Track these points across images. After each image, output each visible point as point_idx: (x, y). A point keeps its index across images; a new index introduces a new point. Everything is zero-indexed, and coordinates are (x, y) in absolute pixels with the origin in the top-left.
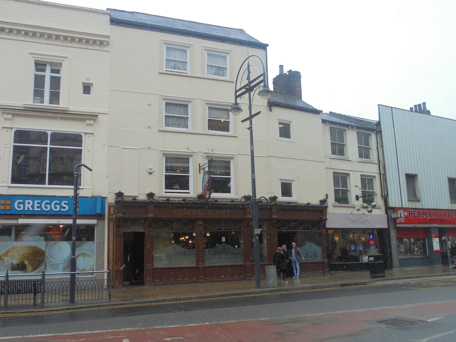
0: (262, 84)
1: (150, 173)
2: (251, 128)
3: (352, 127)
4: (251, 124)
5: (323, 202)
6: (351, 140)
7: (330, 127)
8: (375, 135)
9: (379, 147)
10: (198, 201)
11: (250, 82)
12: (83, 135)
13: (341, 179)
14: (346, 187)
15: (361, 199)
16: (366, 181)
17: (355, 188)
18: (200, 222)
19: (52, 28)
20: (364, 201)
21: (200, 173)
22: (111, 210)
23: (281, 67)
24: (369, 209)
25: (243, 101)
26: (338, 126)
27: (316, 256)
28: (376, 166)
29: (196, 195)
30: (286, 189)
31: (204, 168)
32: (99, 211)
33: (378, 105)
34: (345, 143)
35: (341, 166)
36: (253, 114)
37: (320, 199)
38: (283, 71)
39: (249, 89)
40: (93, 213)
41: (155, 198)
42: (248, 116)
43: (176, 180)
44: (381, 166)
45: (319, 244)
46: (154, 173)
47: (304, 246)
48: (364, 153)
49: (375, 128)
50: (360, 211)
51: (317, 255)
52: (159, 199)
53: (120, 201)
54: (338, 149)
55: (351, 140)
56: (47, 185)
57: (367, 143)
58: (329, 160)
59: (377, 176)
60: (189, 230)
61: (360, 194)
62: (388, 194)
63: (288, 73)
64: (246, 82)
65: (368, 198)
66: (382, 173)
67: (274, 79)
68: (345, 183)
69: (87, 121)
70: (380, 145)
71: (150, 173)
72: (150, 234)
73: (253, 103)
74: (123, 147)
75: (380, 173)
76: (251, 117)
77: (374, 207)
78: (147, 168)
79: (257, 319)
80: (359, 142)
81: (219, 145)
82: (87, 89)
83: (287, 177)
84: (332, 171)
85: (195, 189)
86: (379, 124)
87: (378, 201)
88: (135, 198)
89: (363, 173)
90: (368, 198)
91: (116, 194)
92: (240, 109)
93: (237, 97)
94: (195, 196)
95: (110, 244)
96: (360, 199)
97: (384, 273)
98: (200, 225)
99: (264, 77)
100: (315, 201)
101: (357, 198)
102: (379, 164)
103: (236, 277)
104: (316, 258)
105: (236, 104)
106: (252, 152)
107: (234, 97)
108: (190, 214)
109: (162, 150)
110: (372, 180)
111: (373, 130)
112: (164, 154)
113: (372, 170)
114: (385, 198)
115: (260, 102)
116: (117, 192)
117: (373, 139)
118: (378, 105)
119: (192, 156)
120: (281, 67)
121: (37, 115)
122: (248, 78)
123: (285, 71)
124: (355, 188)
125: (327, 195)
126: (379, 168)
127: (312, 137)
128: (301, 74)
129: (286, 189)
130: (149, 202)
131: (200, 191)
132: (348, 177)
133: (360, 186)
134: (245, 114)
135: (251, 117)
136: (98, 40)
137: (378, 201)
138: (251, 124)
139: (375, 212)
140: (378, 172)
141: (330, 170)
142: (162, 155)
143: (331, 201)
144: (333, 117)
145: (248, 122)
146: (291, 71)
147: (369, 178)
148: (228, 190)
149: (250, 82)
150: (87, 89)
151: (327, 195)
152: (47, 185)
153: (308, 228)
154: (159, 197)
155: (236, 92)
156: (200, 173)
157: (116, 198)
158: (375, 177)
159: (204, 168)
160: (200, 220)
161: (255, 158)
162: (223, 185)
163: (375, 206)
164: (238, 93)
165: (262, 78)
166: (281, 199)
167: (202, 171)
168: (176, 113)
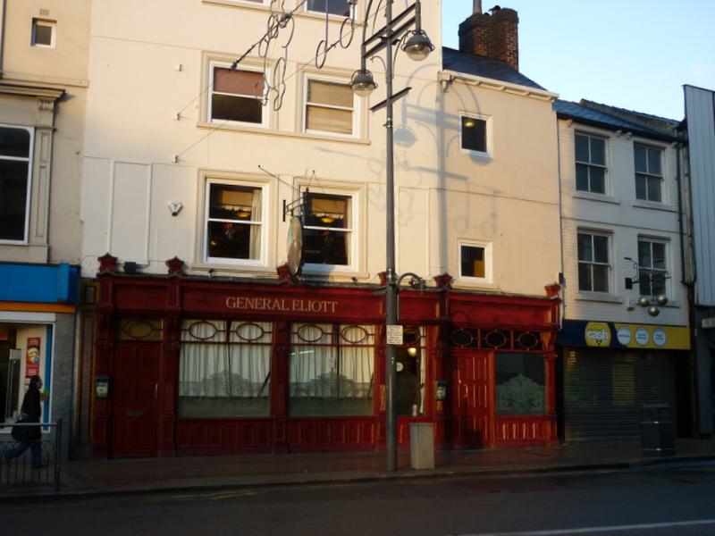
0: (413, 27)
2: (391, 123)
3: (625, 131)
4: (390, 115)
5: (553, 289)
6: (619, 155)
7: (576, 131)
8: (675, 150)
9: (682, 177)
11: (391, 23)
13: (592, 245)
14: (606, 261)
15: (636, 287)
16: (650, 249)
17: (622, 260)
20: (644, 291)
21: (284, 220)
24: (653, 310)
25: (376, 67)
26: (592, 125)
27: (533, 405)
28: (674, 218)
29: (274, 266)
31: (292, 211)
33: (685, 86)
35: (598, 215)
36: (394, 93)
38: (480, 7)
39: (388, 38)
42: (384, 97)
44: (684, 217)
48: (647, 185)
49: (676, 135)
50: (633, 312)
51: (534, 402)
53: (107, 274)
54: (590, 176)
55: (619, 155)
57: (656, 165)
59: (675, 238)
61: (634, 274)
62: (695, 277)
63: (490, 13)
64: (382, 22)
65: (650, 283)
66: (685, 231)
67: (462, 26)
68: (602, 253)
70: (683, 175)
73: (397, 70)
75: (681, 233)
76: (393, 97)
77: (664, 303)
78: (169, 203)
79: (651, 449)
80: (639, 163)
82: (41, 34)
84: (637, 232)
86: (683, 126)
87: (673, 290)
89: (643, 232)
90: (650, 283)
92: (373, 83)
93: (365, 56)
95: (85, 365)
96: (634, 285)
99: (419, 12)
100: (537, 289)
101: (629, 284)
102: (680, 213)
104: (532, 408)
105: (363, 71)
106: (560, 208)
107: (360, 56)
110: (605, 239)
111: (668, 139)
113: (662, 223)
114: (689, 286)
115: (421, 75)
116: (102, 254)
117: (668, 158)
118: (685, 86)
122: (388, 13)
123: (486, 8)
124: (622, 260)
126: (680, 221)
127: (533, 153)
128: (519, 16)
129: (472, 259)
131: (283, 259)
132: (609, 239)
133: (636, 258)
134: (380, 94)
135: (393, 97)
137: (673, 290)
138: (390, 115)
139: (667, 316)
140: (678, 229)
143: (571, 291)
144: (586, 111)
145: (384, 111)
146: (497, 8)
147: (656, 241)
148: (342, 259)
149: (391, 23)
150: (41, 34)
154: (194, 269)
155: (365, 44)
156: (284, 220)
157: (101, 269)
158: (668, 239)
159: (292, 211)
162: (335, 249)
163: (665, 301)
164: (369, 47)
165: (412, 14)
166: (462, 282)
167: (288, 217)
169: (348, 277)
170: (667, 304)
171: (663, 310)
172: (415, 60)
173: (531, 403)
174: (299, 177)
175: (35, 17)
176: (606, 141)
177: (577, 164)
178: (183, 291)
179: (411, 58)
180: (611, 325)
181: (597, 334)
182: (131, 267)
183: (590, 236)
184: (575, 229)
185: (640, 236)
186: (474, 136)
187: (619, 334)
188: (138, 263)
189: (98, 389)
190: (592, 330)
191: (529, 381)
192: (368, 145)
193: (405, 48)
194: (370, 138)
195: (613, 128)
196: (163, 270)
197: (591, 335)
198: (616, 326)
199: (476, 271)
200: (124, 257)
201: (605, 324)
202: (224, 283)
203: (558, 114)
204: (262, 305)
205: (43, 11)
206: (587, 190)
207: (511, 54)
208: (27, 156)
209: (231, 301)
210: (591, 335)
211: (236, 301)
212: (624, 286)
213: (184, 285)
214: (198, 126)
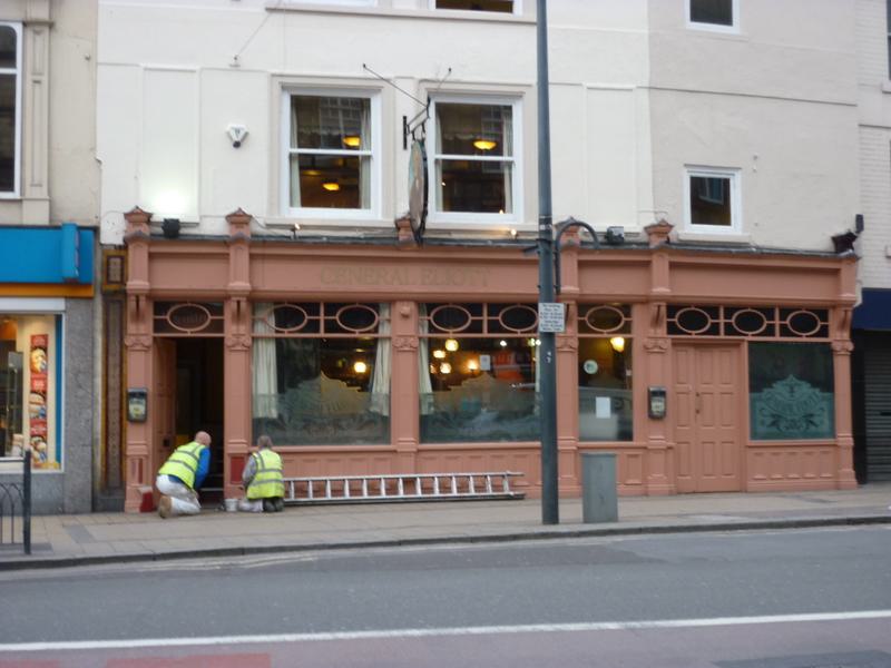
1: (237, 145)
12: (18, 28)
18: (407, 308)
22: (112, 267)
27: (812, 422)
30: (710, 199)
32: (71, 269)
37: (833, 234)
40: (59, 280)
43: (330, 176)
47: (766, 390)
51: (816, 420)
56: (17, 71)
69: (148, 234)
71: (237, 145)
72: (238, 344)
74: (150, 66)
78: (228, 129)
83: (712, 161)
85: (384, 202)
91: (127, 216)
94: (390, 223)
98: (405, 317)
112: (284, 88)
116: (128, 209)
119: (378, 90)
121: (640, 262)
125: (860, 219)
129: (710, 199)
142: (277, 89)
151: (860, 219)
152: (17, 71)
154: (269, 226)
160: (405, 299)
161: (552, 91)
162: (477, 186)
166: (689, 231)
188: (182, 219)
208: (489, 332)
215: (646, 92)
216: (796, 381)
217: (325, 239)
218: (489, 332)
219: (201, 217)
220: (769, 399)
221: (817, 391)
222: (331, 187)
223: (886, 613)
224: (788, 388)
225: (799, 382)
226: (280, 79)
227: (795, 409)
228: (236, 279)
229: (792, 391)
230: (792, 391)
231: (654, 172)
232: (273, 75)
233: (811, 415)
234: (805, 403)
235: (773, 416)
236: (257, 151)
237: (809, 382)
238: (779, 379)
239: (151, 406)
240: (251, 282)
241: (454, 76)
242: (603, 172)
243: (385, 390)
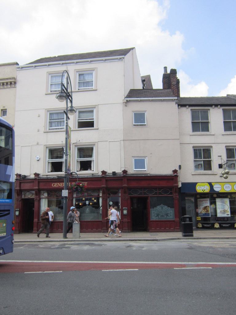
10: (173, 174)
19: (3, 79)
23: (165, 68)
27: (168, 216)
30: (140, 163)
34: (209, 121)
35: (202, 140)
37: (218, 168)
41: (107, 174)
45: (171, 206)
46: (40, 160)
47: (155, 208)
51: (168, 215)
52: (43, 177)
58: (190, 136)
60: (153, 195)
71: (38, 160)
81: (83, 137)
84: (191, 146)
88: (114, 173)
97: (192, 233)
101: (220, 166)
103: (159, 229)
104: (168, 217)
108: (56, 186)
109: (45, 144)
116: (174, 169)
120: (165, 68)
128: (173, 68)
129: (140, 163)
130: (173, 176)
132: (211, 149)
136: (5, 82)
141: (223, 144)
153: (160, 193)
154: (43, 175)
162: (85, 166)
168: (189, 113)
169: (90, 174)
170: (229, 174)
171: (229, 176)
172: (60, 101)
173: (167, 215)
174: (74, 143)
175: (2, 109)
176: (209, 111)
177: (224, 122)
178: (39, 182)
179: (59, 101)
180: (210, 184)
181: (202, 187)
182: (25, 176)
183: (201, 149)
184: (225, 147)
185: (193, 147)
186: (139, 118)
187: (214, 187)
188: (26, 175)
189: (16, 213)
190: (199, 186)
191: (166, 207)
192: (98, 129)
193: (57, 97)
194: (99, 126)
195: (211, 105)
196: (33, 176)
197: (199, 188)
198: (213, 184)
199: (9, 164)
200: (23, 173)
201: (207, 183)
202: (50, 179)
203: (178, 105)
204: (63, 185)
205: (4, 107)
206: (231, 131)
207: (173, 85)
208: (234, 149)
209: (54, 185)
210: (199, 188)
211: (55, 184)
212: (218, 167)
213: (21, 181)
214: (44, 132)
215: (123, 141)
216: (163, 206)
217: (52, 178)
218: (203, 159)
219: (30, 174)
220: (156, 210)
221: (169, 208)
222: (142, 119)
223: (235, 263)
224: (161, 207)
225: (164, 206)
226: (46, 146)
227: (163, 212)
228: (35, 187)
229: (162, 208)
230: (162, 208)
231: (124, 159)
232: (45, 145)
233: (168, 214)
234: (166, 211)
235: (157, 214)
236: (42, 162)
237: (167, 206)
238: (159, 205)
239: (111, 176)
240: (38, 187)
241: (81, 142)
242: (109, 161)
243: (92, 194)
